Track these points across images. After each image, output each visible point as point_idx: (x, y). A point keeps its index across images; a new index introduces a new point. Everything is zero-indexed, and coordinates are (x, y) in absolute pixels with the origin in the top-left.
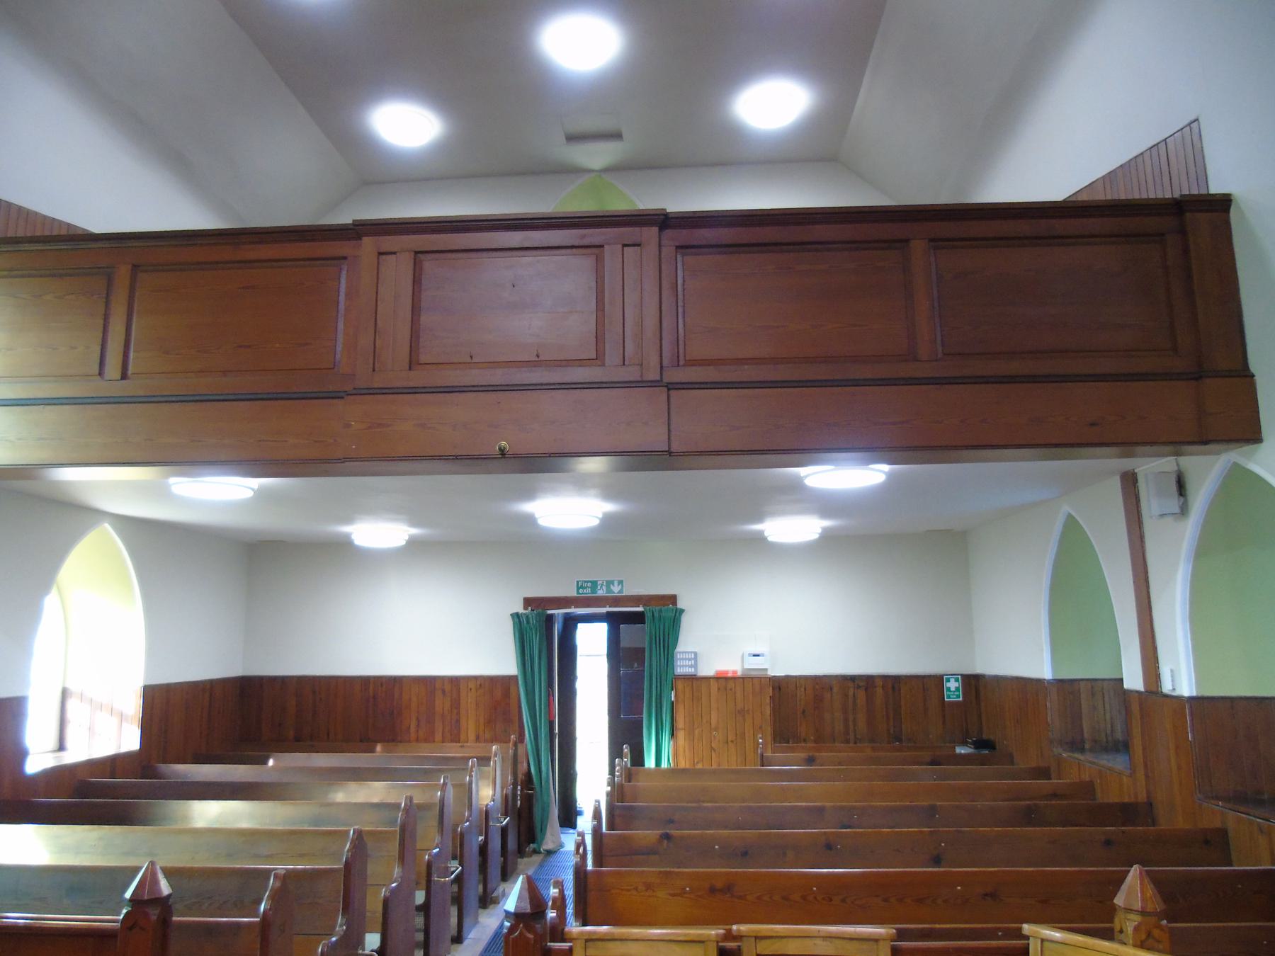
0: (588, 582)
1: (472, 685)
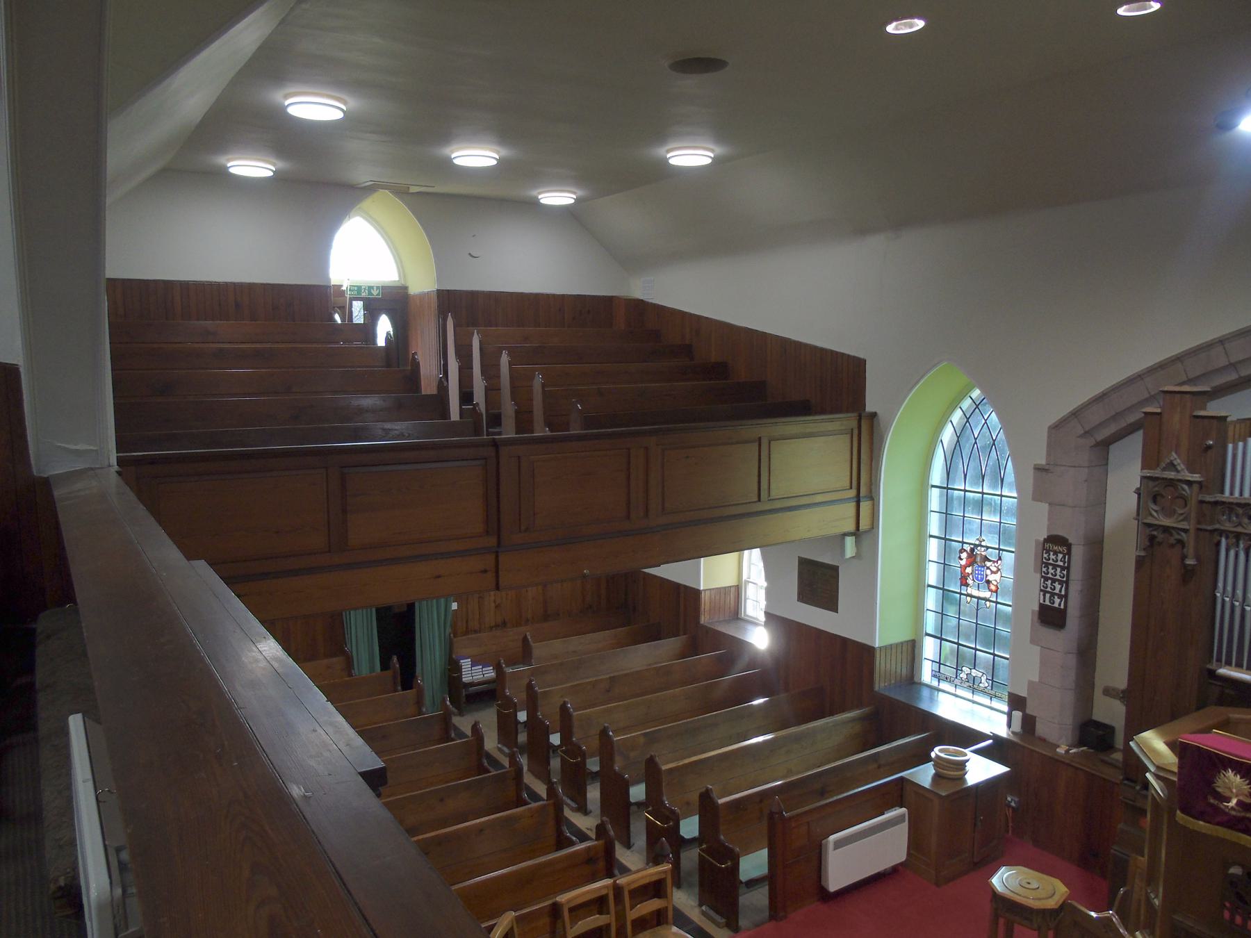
0: (355, 286)
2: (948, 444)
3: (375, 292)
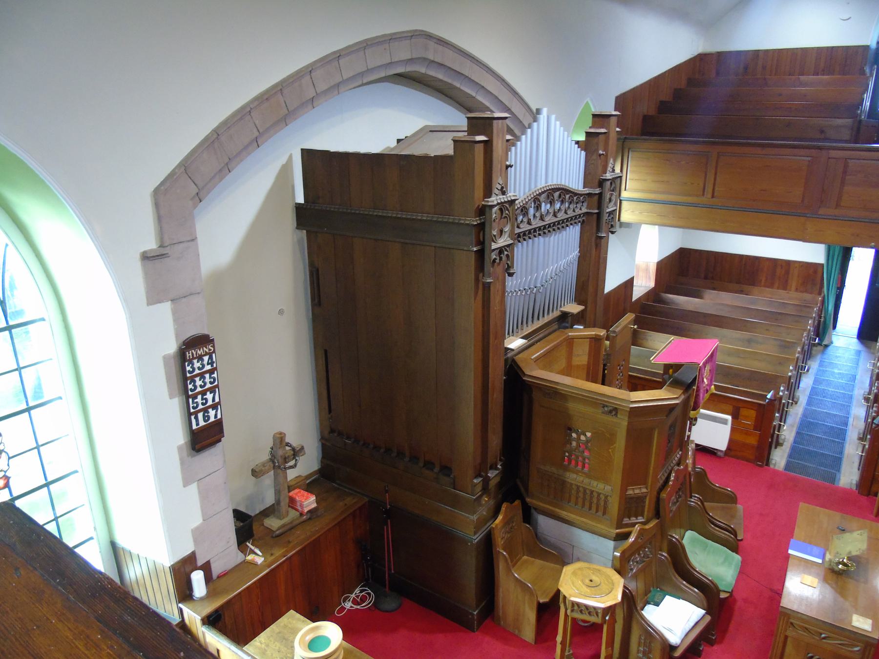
1: (797, 265)
2: (509, 114)
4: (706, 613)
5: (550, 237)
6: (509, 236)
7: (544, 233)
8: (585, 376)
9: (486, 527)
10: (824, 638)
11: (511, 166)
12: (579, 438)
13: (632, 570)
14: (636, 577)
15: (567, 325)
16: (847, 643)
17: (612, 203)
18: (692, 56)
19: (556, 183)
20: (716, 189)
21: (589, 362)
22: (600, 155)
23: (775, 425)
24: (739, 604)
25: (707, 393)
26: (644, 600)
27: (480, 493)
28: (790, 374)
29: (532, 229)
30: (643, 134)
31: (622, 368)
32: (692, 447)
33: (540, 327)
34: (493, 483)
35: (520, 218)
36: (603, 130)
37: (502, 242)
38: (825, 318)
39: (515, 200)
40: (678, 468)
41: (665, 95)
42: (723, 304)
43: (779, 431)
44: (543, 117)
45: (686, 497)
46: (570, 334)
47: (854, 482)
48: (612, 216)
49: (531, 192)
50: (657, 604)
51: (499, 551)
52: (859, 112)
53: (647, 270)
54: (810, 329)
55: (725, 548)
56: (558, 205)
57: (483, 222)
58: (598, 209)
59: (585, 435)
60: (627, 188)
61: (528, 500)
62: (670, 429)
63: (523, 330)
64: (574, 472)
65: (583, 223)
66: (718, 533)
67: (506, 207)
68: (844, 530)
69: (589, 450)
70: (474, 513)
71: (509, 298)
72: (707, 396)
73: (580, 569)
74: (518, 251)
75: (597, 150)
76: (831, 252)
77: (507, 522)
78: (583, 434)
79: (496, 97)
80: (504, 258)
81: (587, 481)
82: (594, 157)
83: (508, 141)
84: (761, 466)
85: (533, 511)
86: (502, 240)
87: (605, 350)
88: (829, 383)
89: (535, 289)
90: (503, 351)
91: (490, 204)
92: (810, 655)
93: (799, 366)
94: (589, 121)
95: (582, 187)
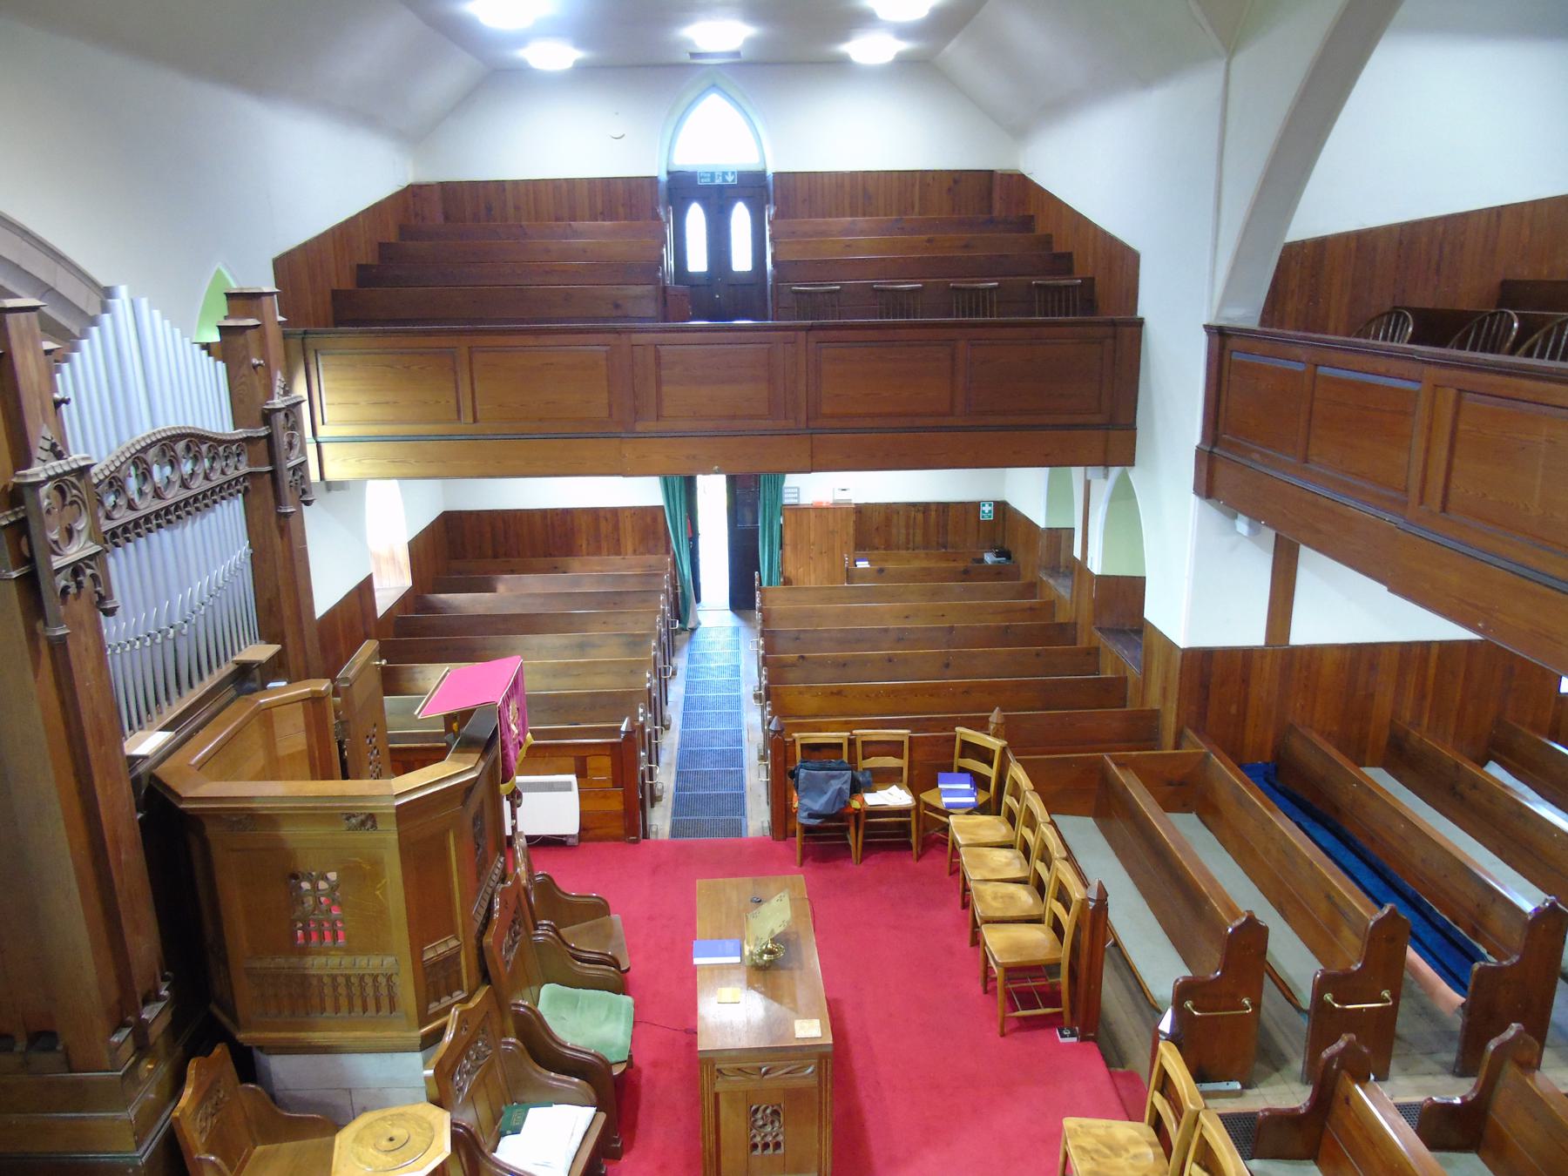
1: (627, 513)
3: (730, 179)
4: (597, 1111)
5: (184, 528)
6: (90, 538)
7: (169, 522)
8: (307, 770)
9: (160, 1123)
10: (766, 1073)
11: (67, 402)
12: (315, 887)
13: (461, 1089)
14: (472, 1098)
15: (253, 685)
16: (796, 1067)
17: (296, 451)
18: (399, 189)
19: (176, 426)
20: (478, 407)
21: (310, 746)
22: (255, 367)
23: (643, 772)
24: (646, 1072)
25: (520, 748)
26: (494, 1134)
27: (133, 1059)
28: (648, 685)
29: (141, 518)
30: (338, 322)
31: (374, 740)
32: (521, 843)
33: (197, 701)
34: (156, 1031)
35: (110, 500)
36: (252, 322)
37: (76, 552)
38: (682, 587)
39: (88, 467)
40: (502, 886)
41: (365, 255)
42: (530, 595)
43: (651, 779)
44: (121, 303)
45: (526, 929)
46: (262, 701)
47: (766, 825)
48: (300, 474)
49: (123, 448)
50: (517, 1131)
51: (199, 1159)
52: (660, 274)
53: (393, 559)
54: (664, 610)
55: (606, 993)
56: (187, 467)
57: (23, 518)
58: (271, 464)
59: (326, 879)
60: (326, 421)
61: (241, 1036)
62: (474, 824)
63: (161, 713)
64: (319, 954)
65: (246, 492)
66: (587, 971)
67: (72, 483)
68: (760, 901)
69: (340, 904)
70: (125, 1105)
71: (118, 658)
72: (522, 752)
73: (369, 1126)
74: (118, 565)
75: (247, 358)
76: (670, 488)
77: (203, 1097)
78: (322, 879)
79: (18, 267)
80: (87, 582)
81: (347, 961)
82: (244, 370)
83: (48, 352)
84: (636, 842)
85: (257, 1053)
86: (75, 549)
87: (336, 712)
88: (706, 685)
89: (172, 631)
90: (123, 768)
91: (30, 480)
92: (753, 1108)
93: (660, 670)
94: (222, 307)
95: (232, 427)
